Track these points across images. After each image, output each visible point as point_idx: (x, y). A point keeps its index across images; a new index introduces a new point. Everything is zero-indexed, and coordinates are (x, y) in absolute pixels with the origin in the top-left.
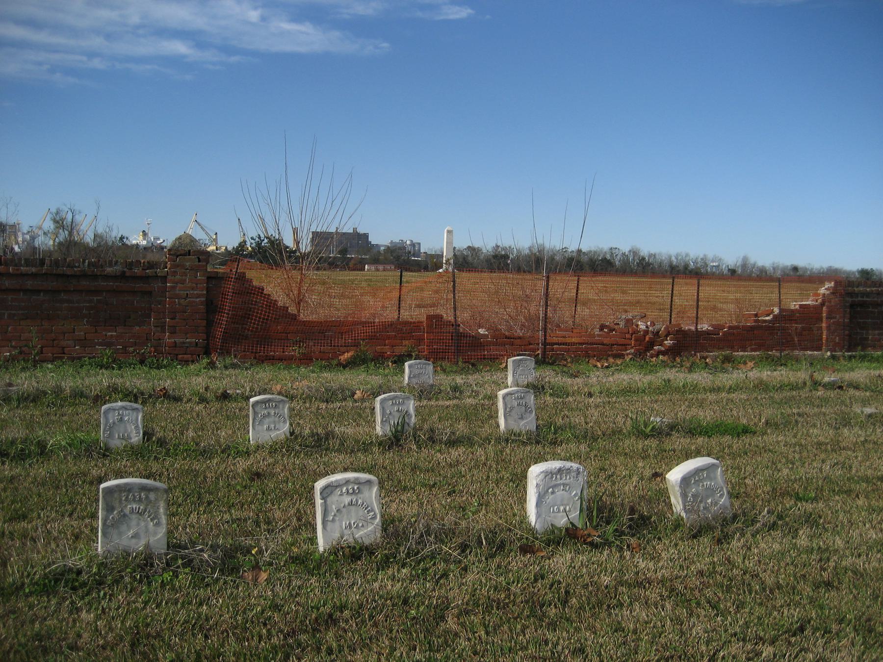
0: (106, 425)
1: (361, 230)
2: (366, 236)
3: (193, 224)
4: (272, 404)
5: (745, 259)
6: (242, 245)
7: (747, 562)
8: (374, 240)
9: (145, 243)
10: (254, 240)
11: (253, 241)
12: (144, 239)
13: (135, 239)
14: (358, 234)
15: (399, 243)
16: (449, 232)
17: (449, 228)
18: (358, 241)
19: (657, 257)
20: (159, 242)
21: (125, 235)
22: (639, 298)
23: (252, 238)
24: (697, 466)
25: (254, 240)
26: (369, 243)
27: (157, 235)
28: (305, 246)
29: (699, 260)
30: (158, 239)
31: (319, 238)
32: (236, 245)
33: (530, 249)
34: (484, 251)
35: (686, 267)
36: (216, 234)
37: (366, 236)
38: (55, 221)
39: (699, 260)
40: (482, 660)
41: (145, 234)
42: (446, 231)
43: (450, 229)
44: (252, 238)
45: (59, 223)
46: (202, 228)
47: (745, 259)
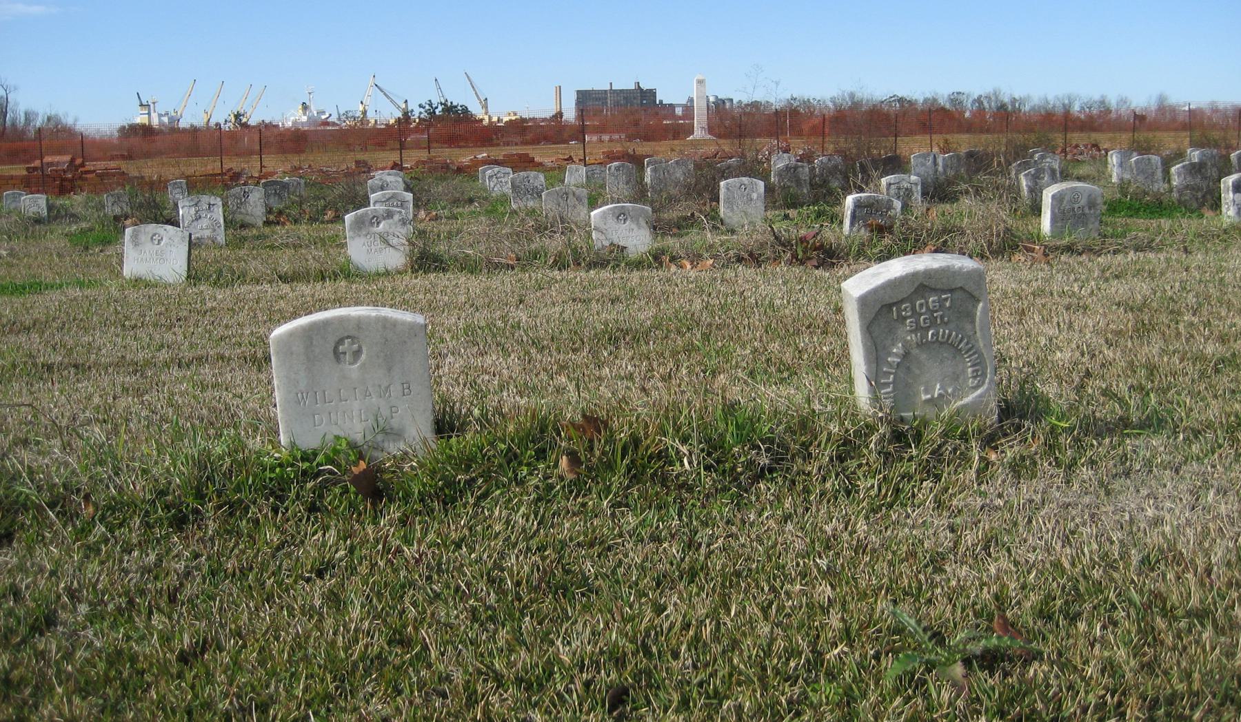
1: (645, 86)
2: (652, 93)
4: (944, 332)
5: (1161, 99)
6: (407, 115)
8: (664, 97)
9: (304, 119)
10: (424, 108)
11: (422, 110)
12: (305, 114)
13: (293, 115)
20: (323, 117)
21: (239, 109)
23: (420, 106)
25: (424, 108)
27: (321, 108)
28: (570, 114)
29: (968, 104)
30: (324, 113)
32: (554, 113)
34: (1153, 109)
35: (1067, 114)
36: (406, 101)
37: (652, 93)
40: (584, 717)
41: (305, 107)
43: (701, 77)
44: (420, 106)
46: (385, 94)
47: (1161, 99)
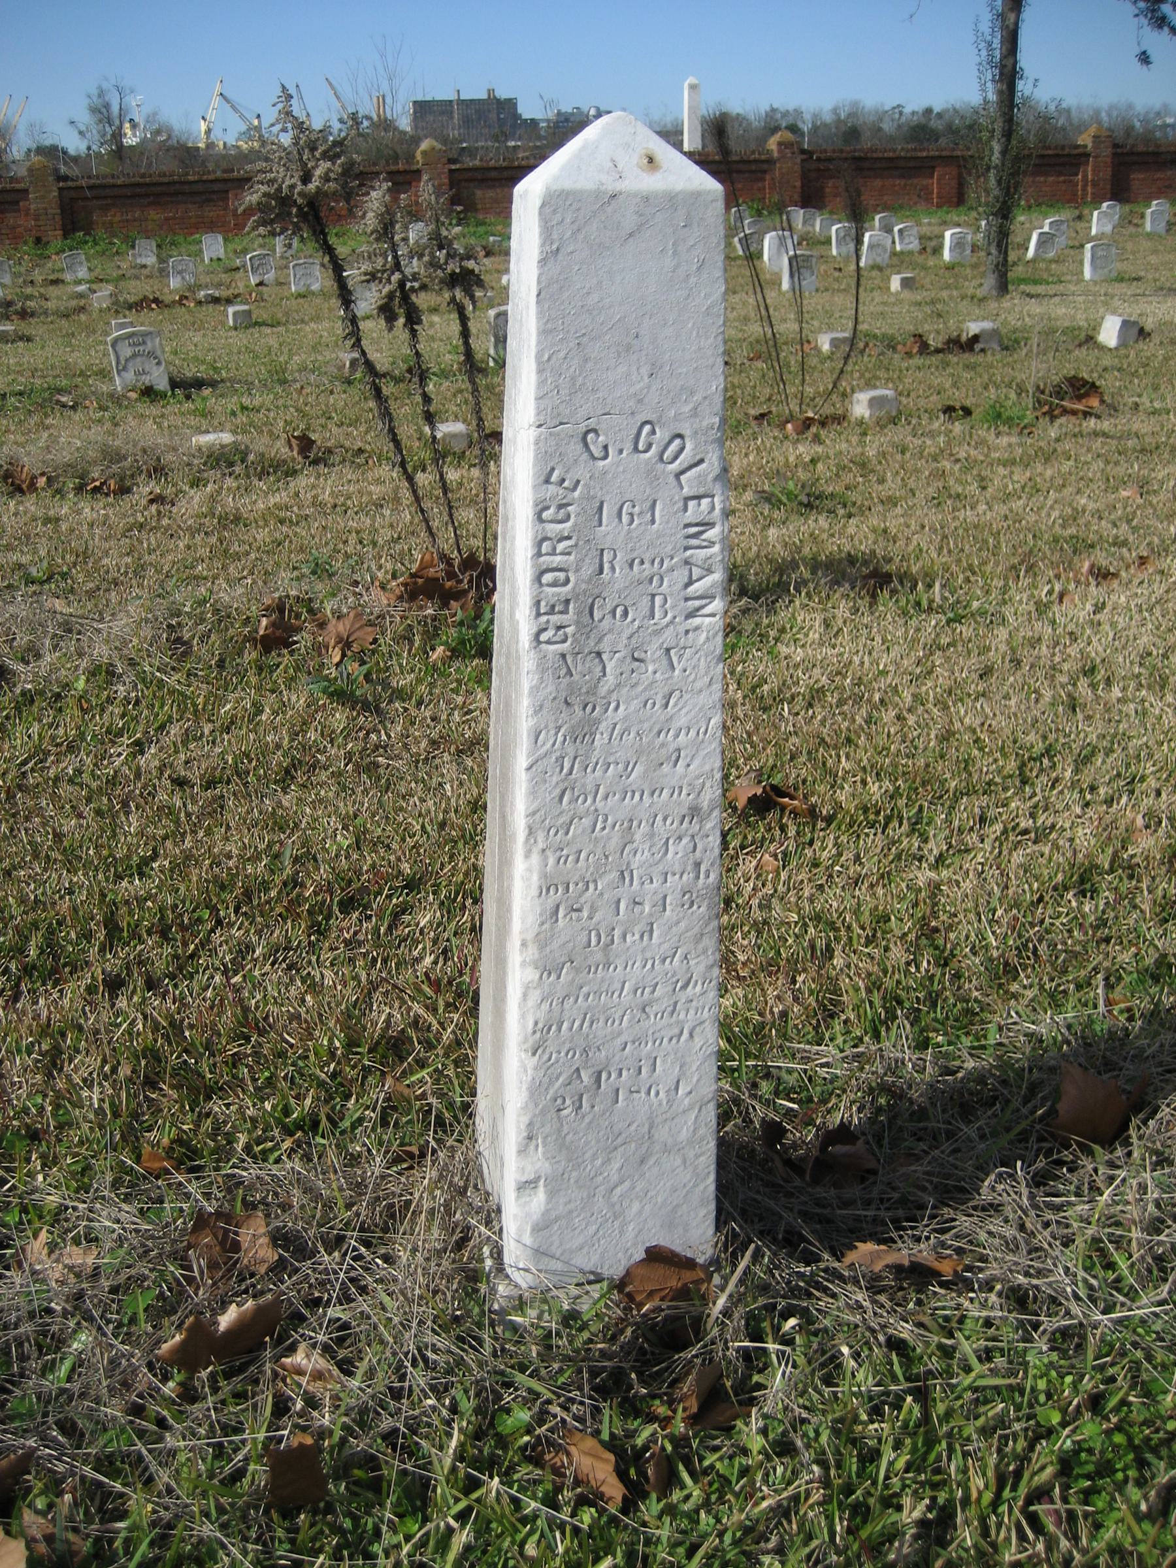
0: (118, 363)
1: (503, 93)
3: (216, 101)
7: (820, 944)
14: (498, 101)
15: (573, 114)
16: (693, 87)
17: (691, 80)
18: (499, 114)
19: (1074, 113)
22: (932, 736)
24: (662, 1243)
26: (516, 116)
31: (422, 108)
33: (835, 111)
36: (258, 116)
38: (94, 110)
39: (807, 117)
42: (686, 85)
45: (101, 111)
46: (233, 107)
